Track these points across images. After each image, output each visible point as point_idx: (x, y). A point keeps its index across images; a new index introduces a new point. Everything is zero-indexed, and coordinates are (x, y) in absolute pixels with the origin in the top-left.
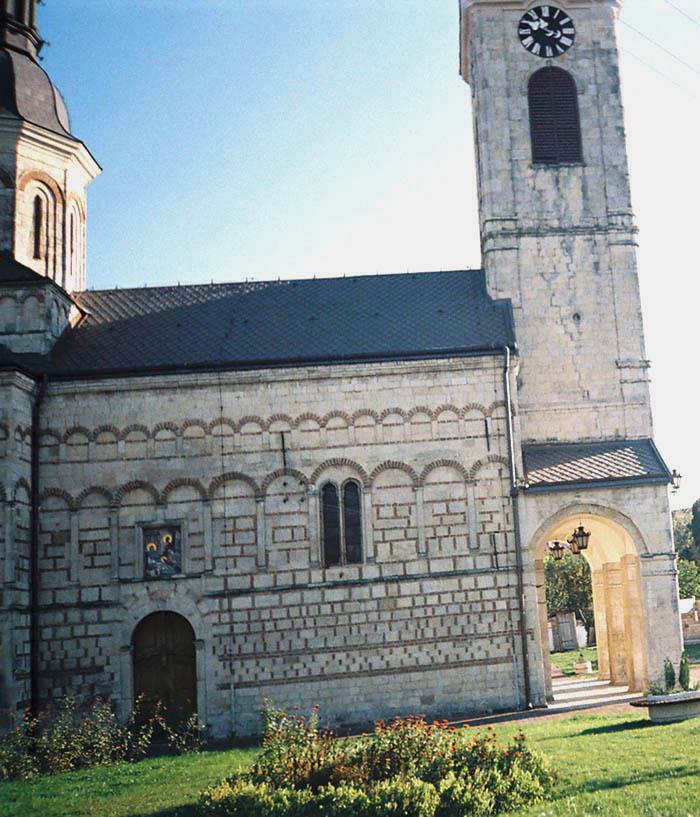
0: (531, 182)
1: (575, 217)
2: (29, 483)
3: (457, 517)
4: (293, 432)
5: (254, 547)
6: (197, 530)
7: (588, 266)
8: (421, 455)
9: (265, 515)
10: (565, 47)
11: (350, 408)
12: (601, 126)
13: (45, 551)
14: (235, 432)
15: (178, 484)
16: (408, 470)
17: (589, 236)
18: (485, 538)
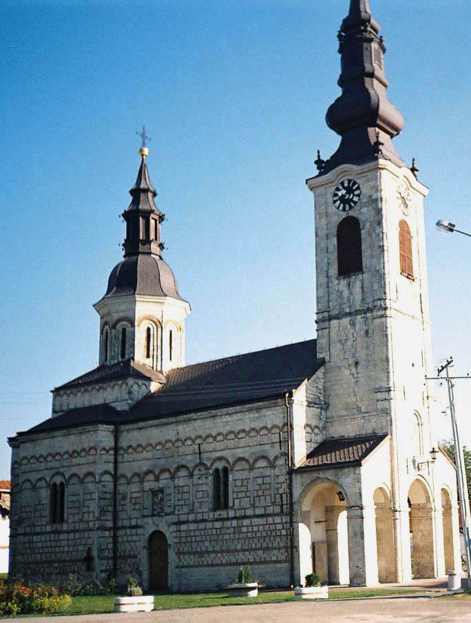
2: (113, 473)
7: (363, 333)
8: (253, 453)
10: (355, 203)
11: (225, 430)
12: (371, 246)
13: (83, 503)
15: (163, 471)
17: (363, 315)
18: (278, 496)
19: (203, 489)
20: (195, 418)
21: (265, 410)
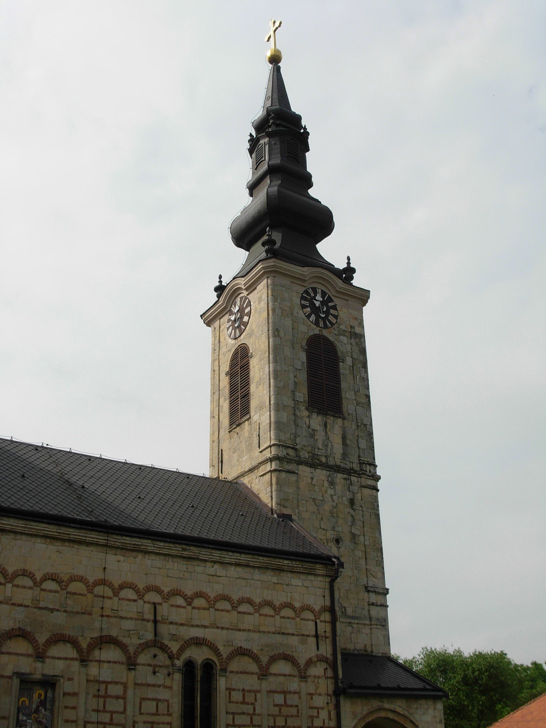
0: (307, 420)
1: (337, 457)
3: (291, 709)
4: (164, 604)
5: (123, 715)
6: (71, 691)
9: (135, 684)
10: (332, 324)
11: (213, 590)
14: (114, 596)
16: (255, 658)
17: (345, 476)
19: (159, 697)
20: (150, 549)
21: (289, 575)
